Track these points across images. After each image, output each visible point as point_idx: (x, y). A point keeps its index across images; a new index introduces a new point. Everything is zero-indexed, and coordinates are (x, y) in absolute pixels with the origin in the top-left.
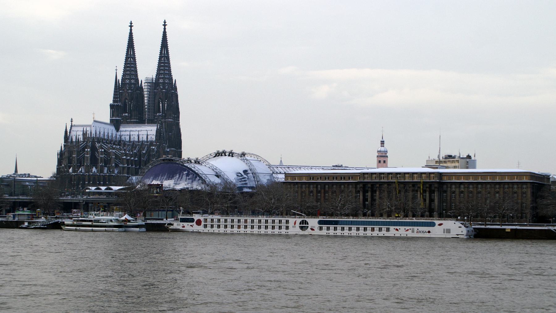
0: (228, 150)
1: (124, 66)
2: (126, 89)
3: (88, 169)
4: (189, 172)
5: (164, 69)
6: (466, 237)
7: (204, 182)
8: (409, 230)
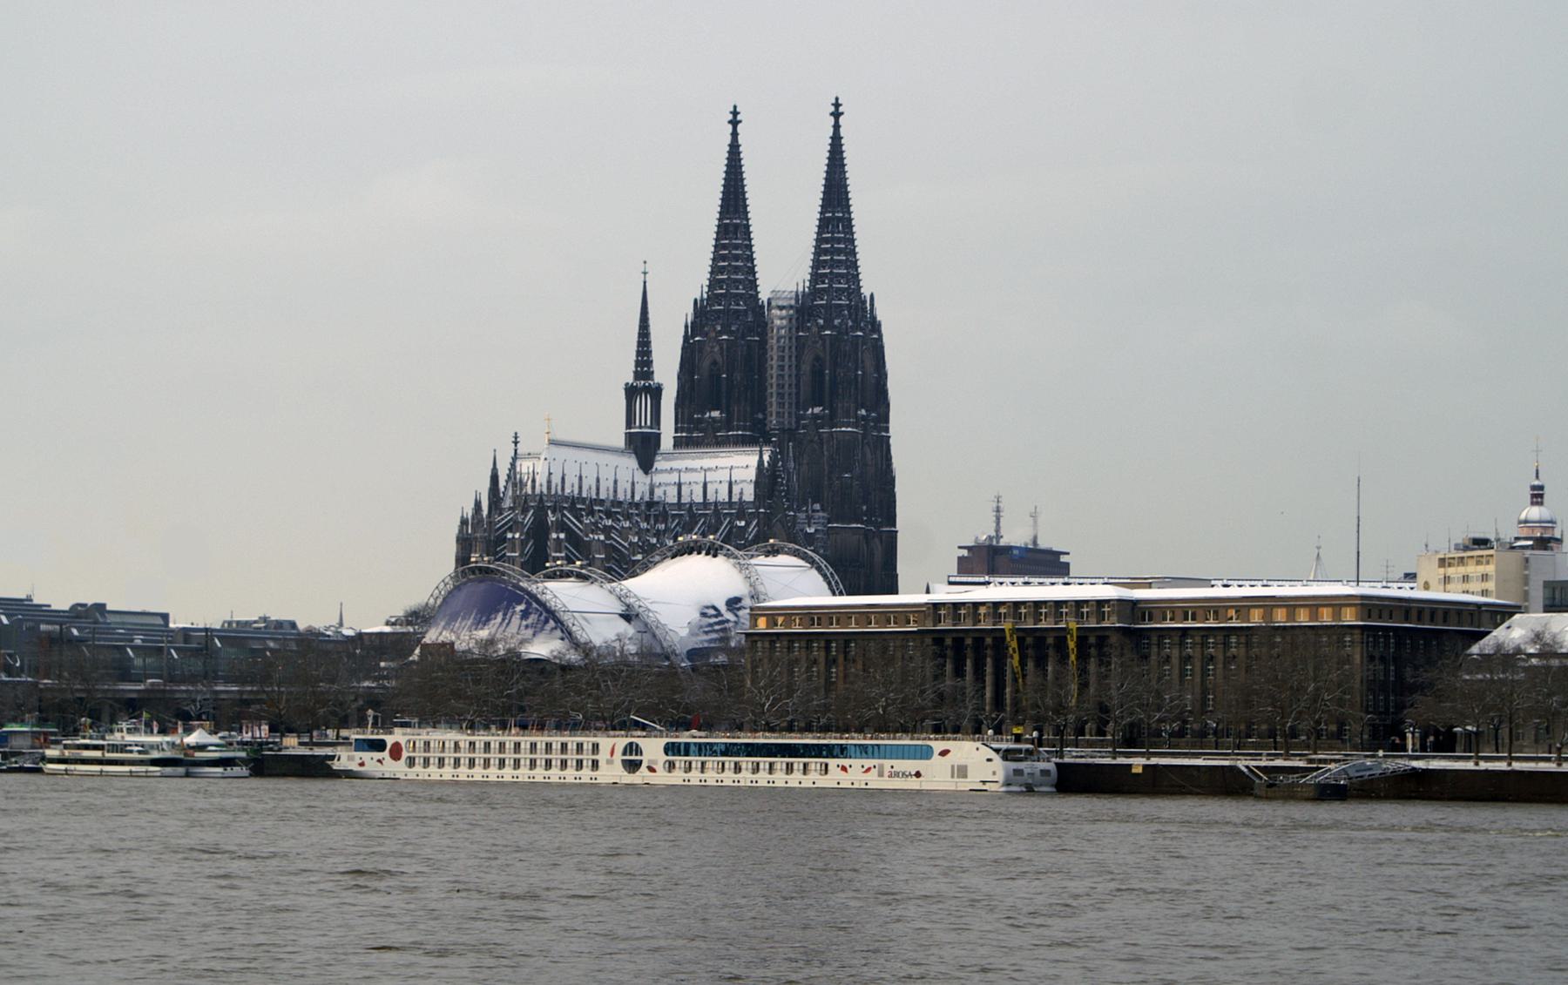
2: (715, 329)
6: (1003, 789)
7: (568, 634)
8: (873, 770)
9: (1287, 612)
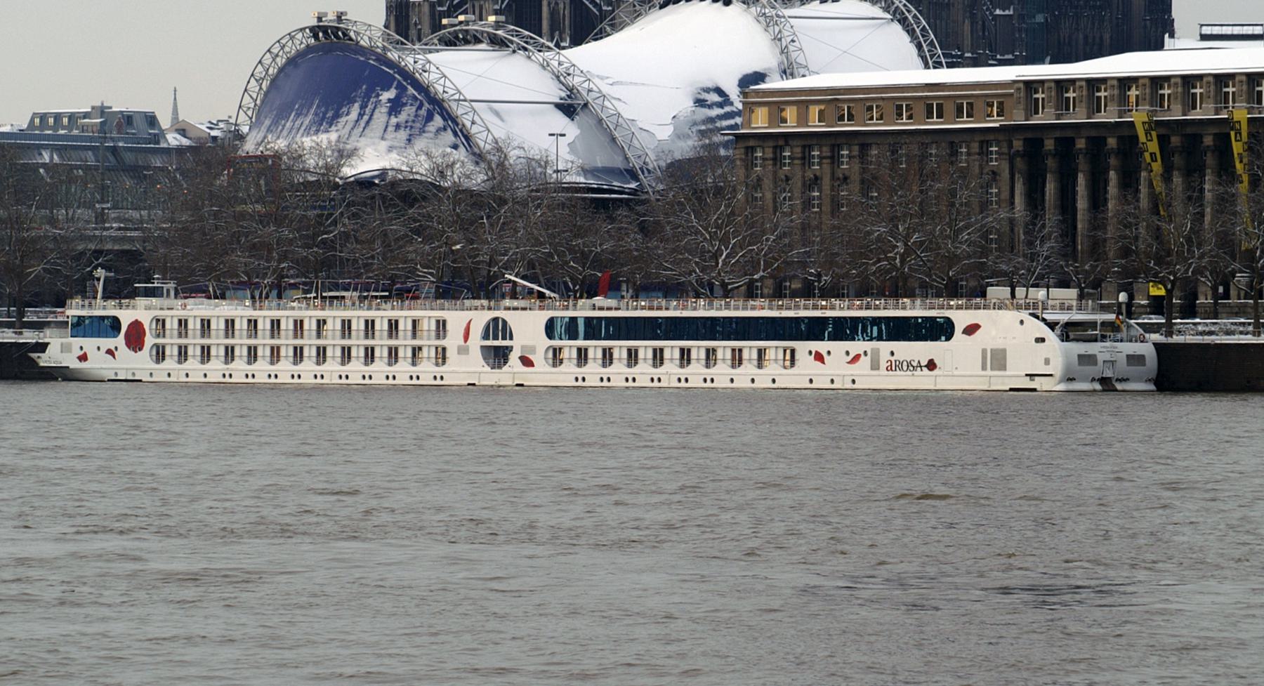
6: (1062, 387)
9: (770, 114)
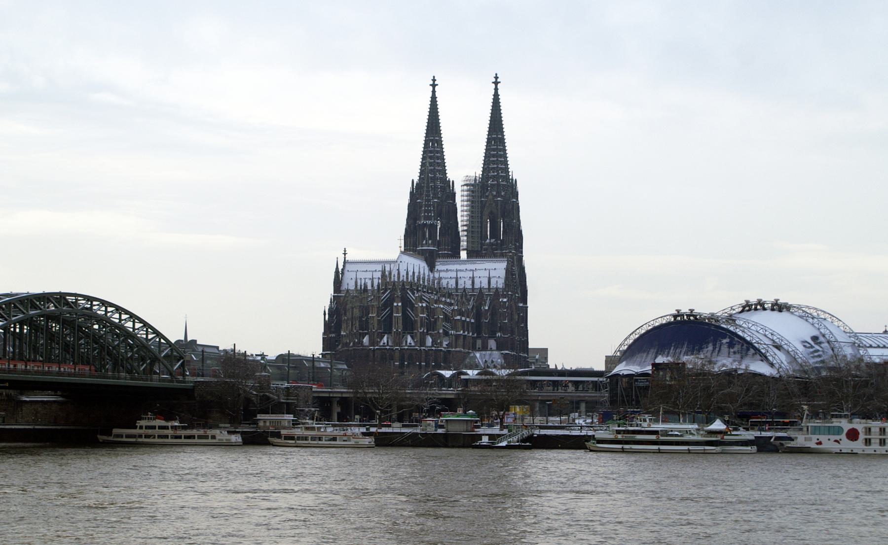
0: (769, 298)
1: (423, 155)
3: (399, 339)
4: (732, 340)
5: (497, 160)
